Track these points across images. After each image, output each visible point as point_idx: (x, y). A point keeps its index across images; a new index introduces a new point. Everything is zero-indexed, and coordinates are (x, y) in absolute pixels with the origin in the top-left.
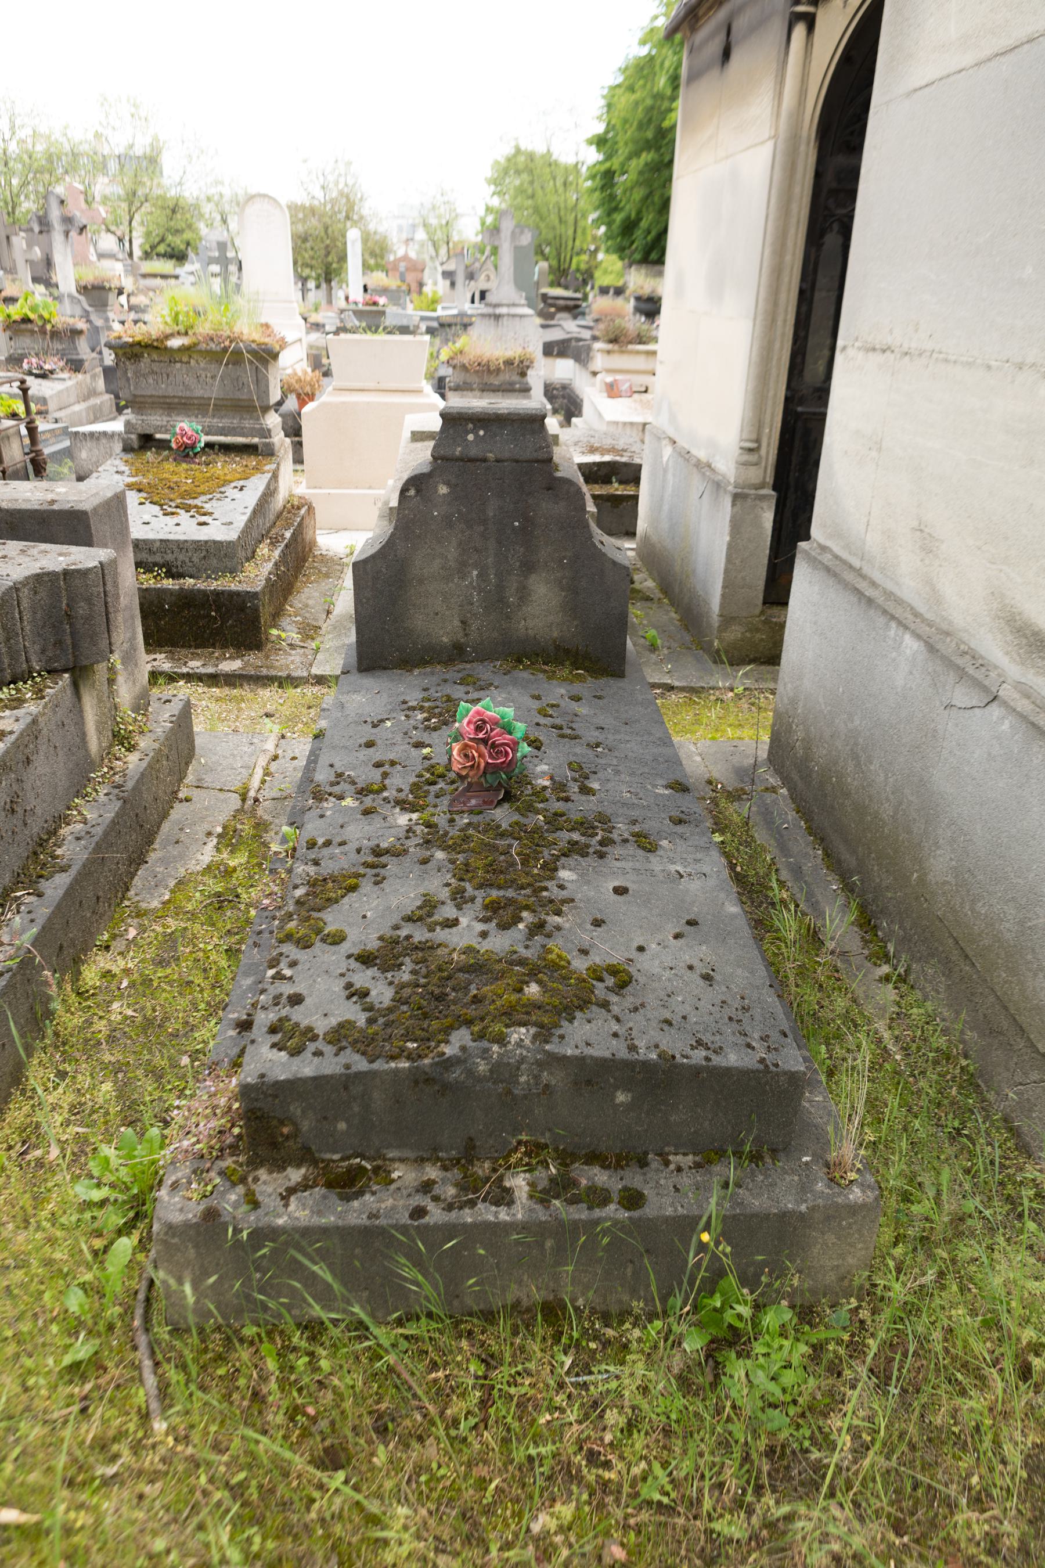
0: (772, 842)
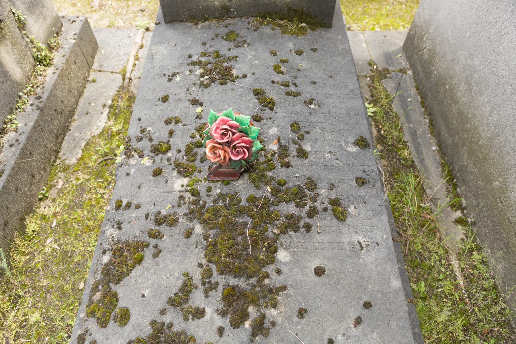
0: (402, 111)
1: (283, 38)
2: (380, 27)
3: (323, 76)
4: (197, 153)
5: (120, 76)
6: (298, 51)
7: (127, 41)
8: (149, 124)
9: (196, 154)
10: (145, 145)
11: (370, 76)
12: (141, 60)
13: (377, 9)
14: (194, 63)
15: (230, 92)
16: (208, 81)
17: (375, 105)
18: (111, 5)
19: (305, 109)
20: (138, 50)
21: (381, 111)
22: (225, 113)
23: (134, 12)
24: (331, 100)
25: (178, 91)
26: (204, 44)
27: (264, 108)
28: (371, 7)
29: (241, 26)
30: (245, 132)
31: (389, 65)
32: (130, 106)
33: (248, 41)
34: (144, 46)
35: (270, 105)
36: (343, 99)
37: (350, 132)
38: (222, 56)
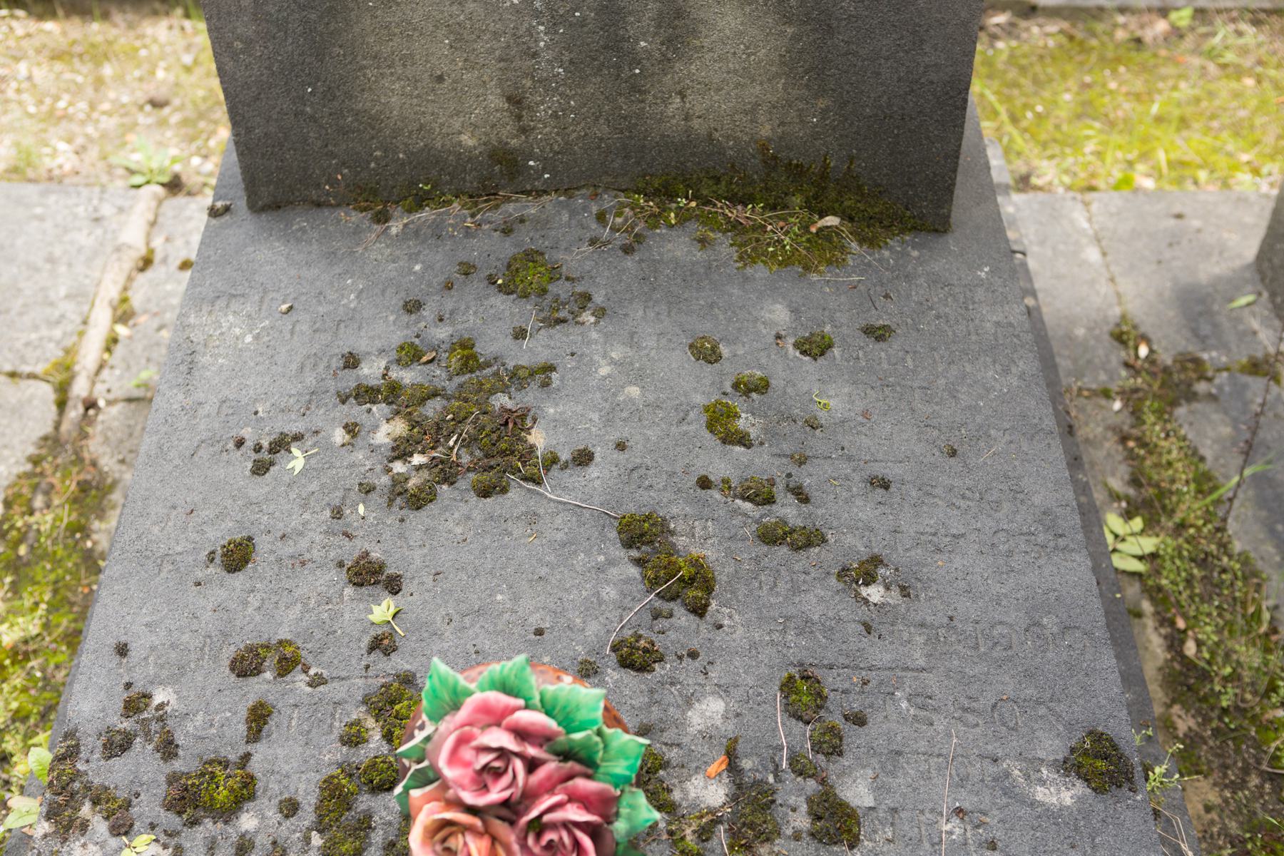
0: (1269, 549)
1: (746, 279)
2: (1156, 173)
3: (919, 449)
4: (368, 816)
5: (46, 392)
6: (807, 340)
7: (85, 238)
8: (164, 674)
9: (365, 824)
10: (141, 772)
11: (1122, 393)
12: (142, 319)
13: (1138, 97)
14: (366, 394)
15: (518, 530)
16: (425, 474)
17: (1151, 526)
18: (30, 78)
19: (845, 609)
20: (130, 279)
21: (1179, 549)
22: (497, 677)
23: (121, 110)
24: (958, 562)
25: (295, 522)
26: (412, 307)
27: (666, 606)
28: (1113, 85)
29: (566, 229)
30: (583, 754)
31: (1203, 340)
32: (80, 529)
33: (599, 298)
34: (158, 258)
35: (688, 587)
36: (1010, 553)
37: (1042, 711)
38: (488, 364)
